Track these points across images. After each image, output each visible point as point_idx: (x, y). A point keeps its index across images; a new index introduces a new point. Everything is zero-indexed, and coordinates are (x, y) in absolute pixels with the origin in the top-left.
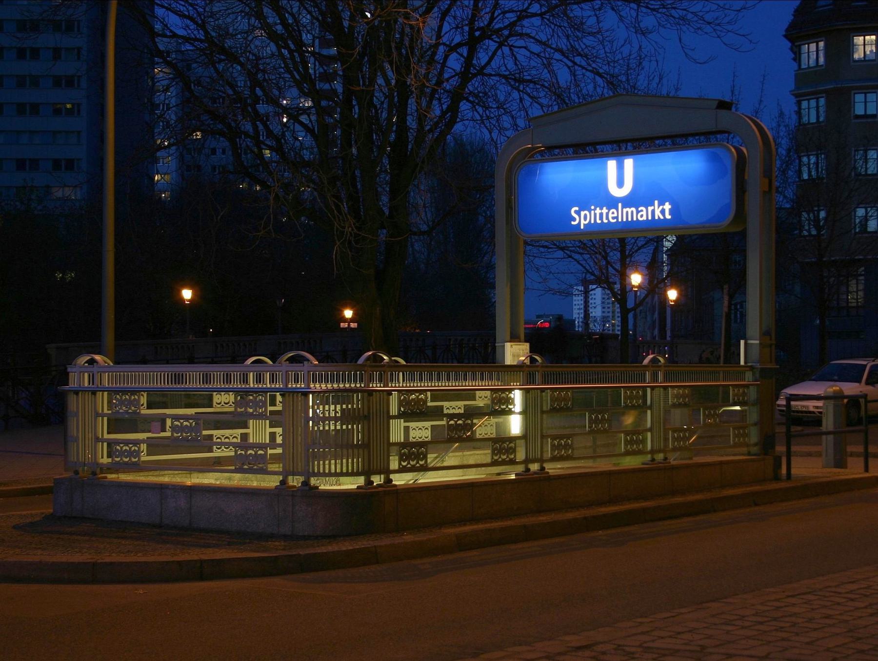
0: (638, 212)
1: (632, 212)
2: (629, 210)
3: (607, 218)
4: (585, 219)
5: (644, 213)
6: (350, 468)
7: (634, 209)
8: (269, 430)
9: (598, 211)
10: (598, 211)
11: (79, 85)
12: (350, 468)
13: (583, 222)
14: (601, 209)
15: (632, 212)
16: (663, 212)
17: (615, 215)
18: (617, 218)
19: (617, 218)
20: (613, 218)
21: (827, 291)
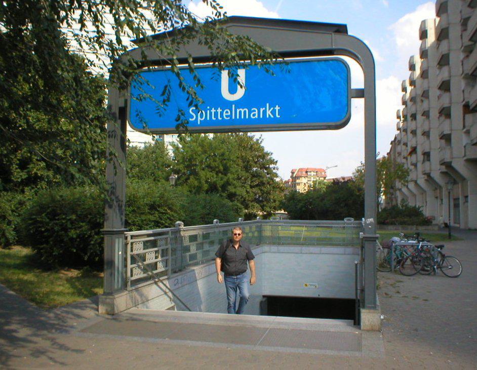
5: (256, 113)
10: (213, 111)
14: (216, 109)
15: (245, 112)
16: (273, 112)
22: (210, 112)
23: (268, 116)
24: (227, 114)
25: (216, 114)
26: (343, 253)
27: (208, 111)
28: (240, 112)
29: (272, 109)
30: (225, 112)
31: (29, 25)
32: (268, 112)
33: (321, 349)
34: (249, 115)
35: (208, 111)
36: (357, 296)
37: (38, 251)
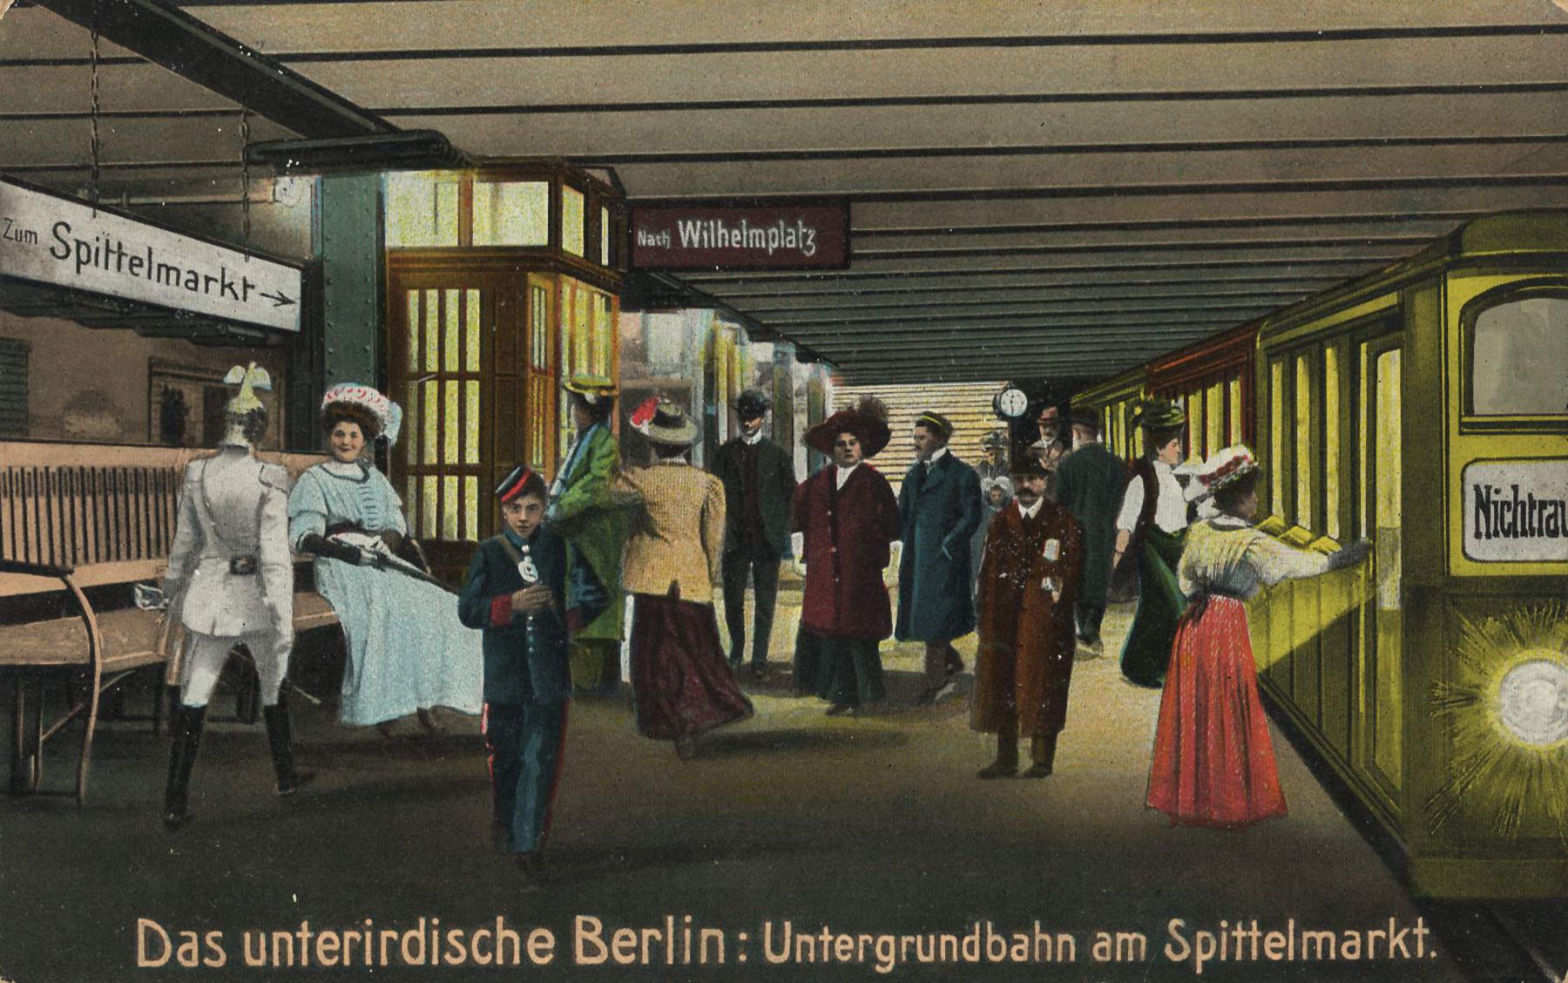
0: (1341, 940)
1: (1326, 941)
2: (1319, 936)
3: (524, 952)
4: (414, 942)
5: (1357, 943)
6: (1037, 953)
7: (1331, 935)
8: (711, 324)
9: (1239, 933)
10: (1239, 933)
11: (168, 552)
12: (1037, 953)
13: (1201, 957)
14: (1247, 928)
15: (1326, 941)
16: (1410, 940)
17: (1282, 945)
18: (1285, 950)
19: (1285, 950)
20: (329, 954)
21: (164, 726)
22: (1229, 936)
23: (1392, 955)
24: (329, 947)
25: (819, 945)
26: (854, 205)
27: (1224, 935)
28: (1312, 941)
29: (1405, 931)
30: (320, 940)
31: (117, 634)
32: (1397, 941)
33: (1244, 626)
34: (524, 952)
35: (1224, 935)
36: (496, 195)
37: (535, 270)
